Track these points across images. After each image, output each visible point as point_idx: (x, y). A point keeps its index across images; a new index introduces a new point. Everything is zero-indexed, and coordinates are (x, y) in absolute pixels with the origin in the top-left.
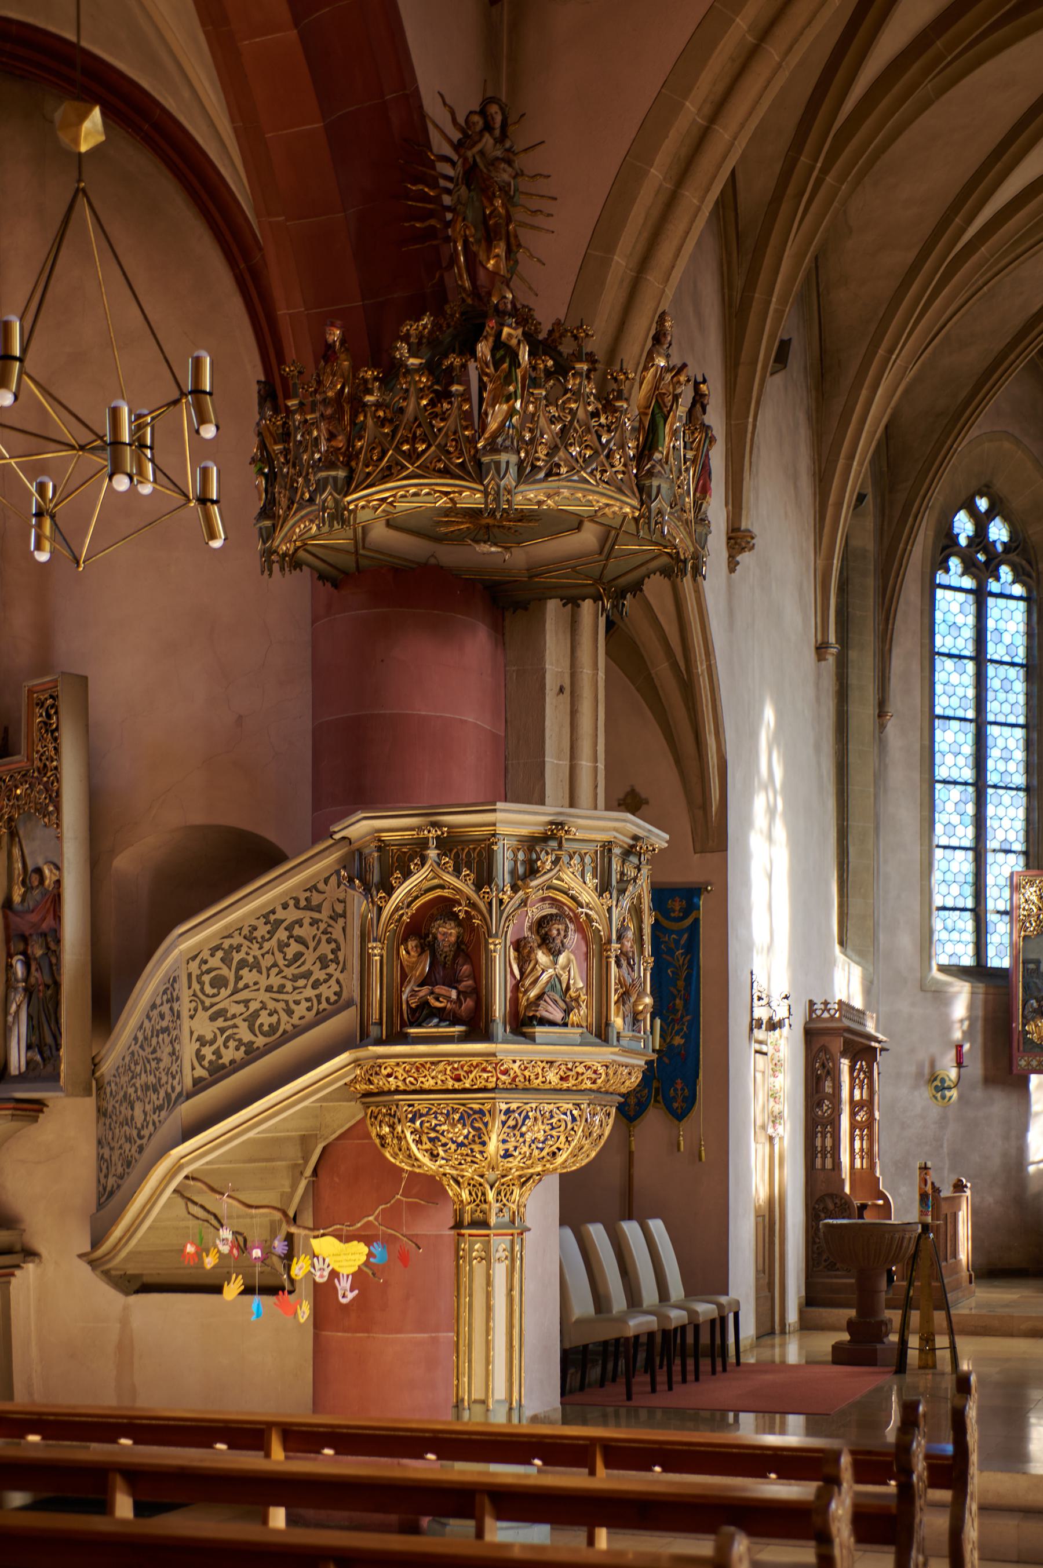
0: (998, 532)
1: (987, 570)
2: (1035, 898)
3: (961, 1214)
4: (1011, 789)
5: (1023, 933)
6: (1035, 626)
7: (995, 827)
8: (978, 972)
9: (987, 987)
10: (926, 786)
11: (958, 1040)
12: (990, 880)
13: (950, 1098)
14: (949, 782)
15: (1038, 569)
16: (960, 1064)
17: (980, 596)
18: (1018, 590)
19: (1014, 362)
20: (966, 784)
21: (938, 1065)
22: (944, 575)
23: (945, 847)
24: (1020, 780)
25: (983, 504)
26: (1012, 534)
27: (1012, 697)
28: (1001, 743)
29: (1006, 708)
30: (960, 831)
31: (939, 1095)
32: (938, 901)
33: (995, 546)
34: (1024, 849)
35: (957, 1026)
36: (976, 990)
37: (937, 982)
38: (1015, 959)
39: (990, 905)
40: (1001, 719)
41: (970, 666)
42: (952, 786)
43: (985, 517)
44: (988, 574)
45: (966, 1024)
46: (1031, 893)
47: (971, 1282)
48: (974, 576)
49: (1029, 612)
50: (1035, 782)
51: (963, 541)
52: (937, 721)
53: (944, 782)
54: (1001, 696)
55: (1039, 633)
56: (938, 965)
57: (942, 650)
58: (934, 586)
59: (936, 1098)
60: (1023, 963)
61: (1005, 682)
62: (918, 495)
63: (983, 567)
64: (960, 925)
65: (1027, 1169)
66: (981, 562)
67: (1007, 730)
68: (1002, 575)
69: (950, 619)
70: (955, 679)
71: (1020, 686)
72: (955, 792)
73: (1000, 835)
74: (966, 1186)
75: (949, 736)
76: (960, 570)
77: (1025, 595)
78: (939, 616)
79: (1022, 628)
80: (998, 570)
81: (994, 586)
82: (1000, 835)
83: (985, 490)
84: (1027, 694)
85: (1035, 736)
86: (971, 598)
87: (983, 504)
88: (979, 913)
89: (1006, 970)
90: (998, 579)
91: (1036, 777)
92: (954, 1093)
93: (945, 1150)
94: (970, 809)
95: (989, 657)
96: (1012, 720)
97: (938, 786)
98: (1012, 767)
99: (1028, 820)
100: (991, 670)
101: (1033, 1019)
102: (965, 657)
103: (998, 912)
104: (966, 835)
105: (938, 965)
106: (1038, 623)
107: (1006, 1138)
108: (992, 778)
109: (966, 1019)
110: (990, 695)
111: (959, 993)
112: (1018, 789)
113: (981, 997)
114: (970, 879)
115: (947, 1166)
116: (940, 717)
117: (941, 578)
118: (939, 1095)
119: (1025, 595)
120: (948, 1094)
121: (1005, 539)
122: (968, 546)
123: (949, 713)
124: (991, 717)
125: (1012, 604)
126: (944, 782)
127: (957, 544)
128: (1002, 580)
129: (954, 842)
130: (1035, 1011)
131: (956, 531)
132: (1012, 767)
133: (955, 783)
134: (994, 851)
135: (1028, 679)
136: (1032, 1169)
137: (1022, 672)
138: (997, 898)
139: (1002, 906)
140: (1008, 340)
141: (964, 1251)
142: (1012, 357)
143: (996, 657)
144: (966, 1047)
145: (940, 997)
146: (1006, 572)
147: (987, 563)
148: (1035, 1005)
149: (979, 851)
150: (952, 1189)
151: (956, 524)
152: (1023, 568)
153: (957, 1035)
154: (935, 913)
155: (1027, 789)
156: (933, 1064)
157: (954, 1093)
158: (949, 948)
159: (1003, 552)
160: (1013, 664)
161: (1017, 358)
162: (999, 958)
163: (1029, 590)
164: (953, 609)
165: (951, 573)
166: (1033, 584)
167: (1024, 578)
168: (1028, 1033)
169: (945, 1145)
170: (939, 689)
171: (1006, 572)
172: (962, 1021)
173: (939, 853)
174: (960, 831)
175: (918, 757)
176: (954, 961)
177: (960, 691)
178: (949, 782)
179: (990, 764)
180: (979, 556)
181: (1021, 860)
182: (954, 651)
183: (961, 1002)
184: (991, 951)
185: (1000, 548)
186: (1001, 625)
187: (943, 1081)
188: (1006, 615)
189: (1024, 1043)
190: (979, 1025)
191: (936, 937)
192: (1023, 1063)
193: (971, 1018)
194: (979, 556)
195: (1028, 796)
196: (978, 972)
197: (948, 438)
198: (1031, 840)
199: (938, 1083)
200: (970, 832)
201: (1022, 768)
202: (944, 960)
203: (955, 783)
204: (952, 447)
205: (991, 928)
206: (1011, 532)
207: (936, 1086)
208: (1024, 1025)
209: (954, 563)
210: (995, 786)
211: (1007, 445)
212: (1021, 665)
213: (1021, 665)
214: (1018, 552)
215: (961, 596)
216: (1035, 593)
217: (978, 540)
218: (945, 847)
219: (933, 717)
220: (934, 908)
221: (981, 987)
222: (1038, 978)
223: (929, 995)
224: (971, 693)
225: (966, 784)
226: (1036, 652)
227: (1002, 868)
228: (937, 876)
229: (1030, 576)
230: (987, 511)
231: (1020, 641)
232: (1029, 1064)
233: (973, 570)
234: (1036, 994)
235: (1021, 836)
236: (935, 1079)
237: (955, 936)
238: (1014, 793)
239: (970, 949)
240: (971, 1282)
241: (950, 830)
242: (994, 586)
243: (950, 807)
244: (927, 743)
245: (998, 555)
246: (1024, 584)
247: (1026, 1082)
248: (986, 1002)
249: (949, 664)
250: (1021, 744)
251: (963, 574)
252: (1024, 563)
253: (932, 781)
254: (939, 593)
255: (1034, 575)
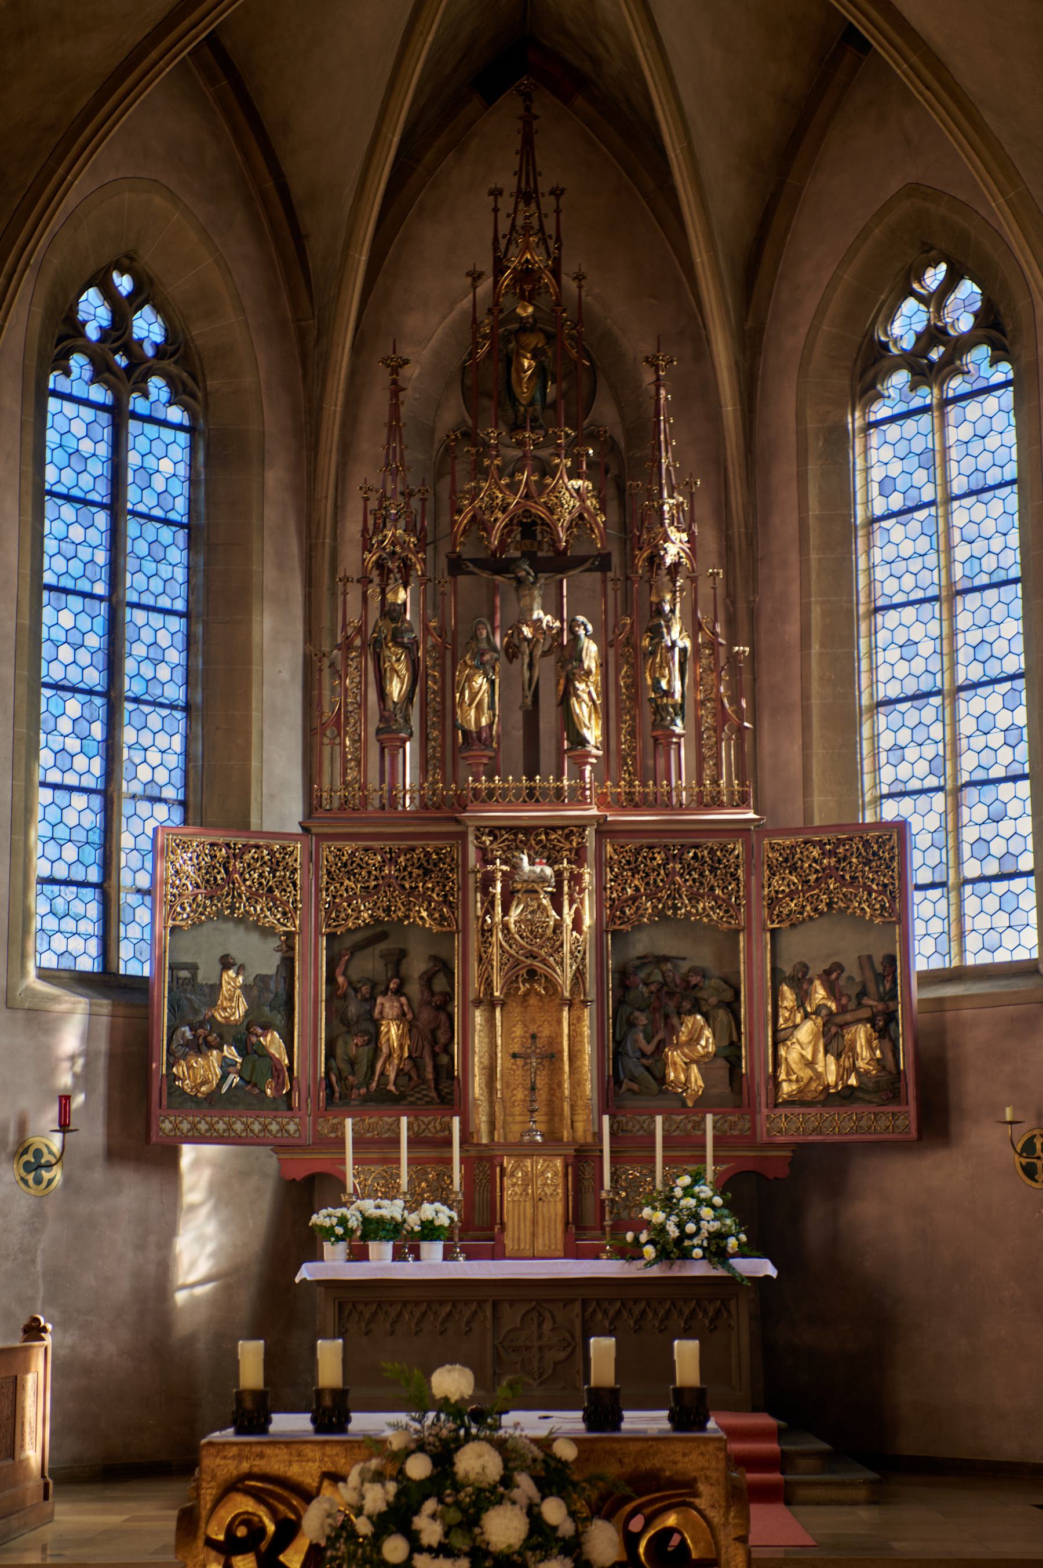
0: (148, 327)
1: (129, 380)
2: (189, 869)
3: (30, 1378)
4: (162, 705)
5: (170, 923)
6: (202, 470)
7: (137, 761)
8: (104, 981)
9: (113, 1005)
10: (23, 689)
11: (66, 1088)
12: (126, 841)
13: (50, 1181)
14: (64, 688)
15: (205, 388)
16: (64, 1126)
17: (118, 415)
18: (176, 414)
19: (157, 63)
20: (90, 692)
21: (31, 1127)
22: (62, 378)
23: (55, 787)
24: (175, 693)
25: (124, 284)
26: (170, 331)
27: (165, 571)
28: (147, 635)
29: (156, 585)
30: (80, 763)
31: (30, 1177)
32: (42, 868)
33: (141, 346)
34: (181, 797)
35: (66, 1065)
36: (96, 1009)
37: (33, 993)
38: (158, 962)
39: (126, 878)
40: (147, 599)
41: (102, 519)
42: (69, 695)
43: (126, 303)
44: (129, 386)
45: (80, 1062)
46: (186, 862)
47: (46, 1497)
48: (110, 386)
49: (193, 448)
50: (199, 698)
51: (92, 332)
52: (45, 594)
53: (56, 686)
54: (149, 567)
55: (206, 480)
56: (39, 968)
57: (57, 488)
58: (42, 394)
59: (25, 1182)
60: (171, 968)
61: (155, 546)
62: (14, 244)
63: (123, 375)
64: (77, 907)
65: (173, 1297)
66: (121, 367)
67: (156, 619)
68: (152, 390)
69: (71, 443)
70: (77, 533)
71: (177, 555)
72: (73, 706)
73: (144, 773)
74: (44, 1330)
75: (66, 619)
76: (87, 374)
77: (186, 422)
78: (52, 437)
79: (182, 470)
80: (145, 381)
81: (138, 404)
82: (144, 773)
83: (126, 262)
84: (188, 568)
85: (199, 629)
86: (104, 418)
87: (124, 284)
88: (106, 891)
89: (147, 978)
90: (146, 395)
91: (200, 690)
92: (57, 1174)
93: (39, 1268)
94: (98, 730)
95: (129, 506)
96: (164, 602)
97: (46, 692)
98: (164, 673)
99: (187, 754)
100: (132, 527)
101: (184, 1057)
102: (93, 503)
103: (139, 891)
104: (89, 769)
105: (39, 968)
106: (206, 466)
107: (140, 1247)
108: (132, 687)
109: (80, 1055)
110: (131, 564)
111: (71, 1012)
112: (172, 707)
113: (105, 1021)
114: (96, 837)
115: (41, 1295)
116: (50, 588)
117: (55, 381)
118: (30, 1177)
119: (186, 422)
120: (46, 1175)
121: (159, 339)
122: (101, 340)
123: (67, 582)
124: (132, 596)
125: (167, 434)
126: (56, 686)
127: (83, 335)
128: (152, 398)
129: (71, 779)
130: (187, 1044)
131: (81, 316)
132: (164, 673)
133: (74, 690)
134: (134, 797)
135: (191, 545)
136: (181, 1297)
137: (181, 535)
138: (134, 872)
139: (144, 881)
140: (147, 31)
141: (34, 1449)
142: (154, 55)
143: (141, 508)
144: (79, 1100)
145: (38, 1019)
146: (157, 386)
147: (129, 370)
148: (189, 1034)
149: (108, 795)
150: (21, 1334)
151: (82, 306)
152: (184, 384)
153: (65, 1080)
154: (35, 888)
155: (187, 708)
156: (22, 1127)
157: (57, 1174)
158: (59, 943)
159: (155, 357)
160: (167, 522)
161: (162, 58)
162: (134, 961)
163: (193, 417)
164: (73, 428)
165: (73, 377)
166: (198, 408)
167: (186, 398)
168: (176, 1078)
169: (39, 1260)
170: (50, 545)
171: (157, 386)
172: (72, 1058)
173: (44, 795)
174: (80, 763)
175: (12, 643)
176: (66, 963)
177: (85, 553)
178: (64, 688)
179: (130, 666)
180: (117, 357)
181: (177, 815)
182: (75, 492)
183: (73, 1031)
184: (125, 951)
185: (149, 351)
186: (150, 462)
187: (38, 1154)
188: (158, 448)
189: (169, 1094)
190: (101, 1064)
191: (36, 924)
192: (167, 1126)
193: (88, 1054)
194: (117, 357)
195: (188, 718)
196: (104, 981)
197: (59, 163)
198: (191, 784)
199: (29, 1157)
200: (97, 766)
201: (179, 675)
202: (49, 961)
203: (74, 690)
204: (64, 179)
205: (126, 915)
206: (166, 330)
207: (27, 1163)
208: (170, 1066)
209: (78, 362)
210: (136, 700)
211: (158, 200)
212: (181, 525)
213: (181, 525)
214: (179, 359)
215: (88, 414)
216: (201, 421)
217: (115, 334)
218: (55, 787)
219: (39, 587)
220: (33, 880)
221: (105, 1006)
222: (194, 992)
223: (20, 1015)
224: (101, 557)
225: (90, 692)
226: (202, 508)
227: (141, 825)
228: (40, 829)
229: (194, 396)
230: (130, 295)
231: (179, 487)
232: (176, 1127)
233: (107, 375)
234: (191, 1017)
235: (178, 777)
236: (25, 1152)
237: (69, 924)
238: (165, 712)
239: (93, 947)
240: (46, 1497)
241: (64, 761)
242: (138, 404)
243: (65, 725)
244: (26, 622)
245: (146, 359)
246: (186, 408)
247: (174, 1156)
248: (112, 1028)
249: (68, 511)
250: (180, 640)
251: (92, 381)
252: (185, 375)
253: (35, 684)
254: (53, 404)
255: (200, 395)
